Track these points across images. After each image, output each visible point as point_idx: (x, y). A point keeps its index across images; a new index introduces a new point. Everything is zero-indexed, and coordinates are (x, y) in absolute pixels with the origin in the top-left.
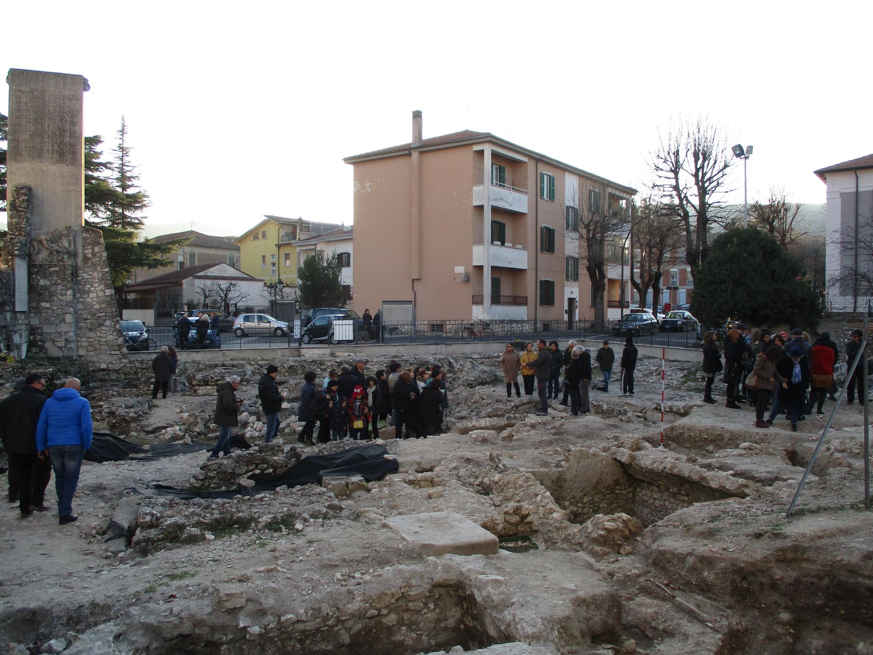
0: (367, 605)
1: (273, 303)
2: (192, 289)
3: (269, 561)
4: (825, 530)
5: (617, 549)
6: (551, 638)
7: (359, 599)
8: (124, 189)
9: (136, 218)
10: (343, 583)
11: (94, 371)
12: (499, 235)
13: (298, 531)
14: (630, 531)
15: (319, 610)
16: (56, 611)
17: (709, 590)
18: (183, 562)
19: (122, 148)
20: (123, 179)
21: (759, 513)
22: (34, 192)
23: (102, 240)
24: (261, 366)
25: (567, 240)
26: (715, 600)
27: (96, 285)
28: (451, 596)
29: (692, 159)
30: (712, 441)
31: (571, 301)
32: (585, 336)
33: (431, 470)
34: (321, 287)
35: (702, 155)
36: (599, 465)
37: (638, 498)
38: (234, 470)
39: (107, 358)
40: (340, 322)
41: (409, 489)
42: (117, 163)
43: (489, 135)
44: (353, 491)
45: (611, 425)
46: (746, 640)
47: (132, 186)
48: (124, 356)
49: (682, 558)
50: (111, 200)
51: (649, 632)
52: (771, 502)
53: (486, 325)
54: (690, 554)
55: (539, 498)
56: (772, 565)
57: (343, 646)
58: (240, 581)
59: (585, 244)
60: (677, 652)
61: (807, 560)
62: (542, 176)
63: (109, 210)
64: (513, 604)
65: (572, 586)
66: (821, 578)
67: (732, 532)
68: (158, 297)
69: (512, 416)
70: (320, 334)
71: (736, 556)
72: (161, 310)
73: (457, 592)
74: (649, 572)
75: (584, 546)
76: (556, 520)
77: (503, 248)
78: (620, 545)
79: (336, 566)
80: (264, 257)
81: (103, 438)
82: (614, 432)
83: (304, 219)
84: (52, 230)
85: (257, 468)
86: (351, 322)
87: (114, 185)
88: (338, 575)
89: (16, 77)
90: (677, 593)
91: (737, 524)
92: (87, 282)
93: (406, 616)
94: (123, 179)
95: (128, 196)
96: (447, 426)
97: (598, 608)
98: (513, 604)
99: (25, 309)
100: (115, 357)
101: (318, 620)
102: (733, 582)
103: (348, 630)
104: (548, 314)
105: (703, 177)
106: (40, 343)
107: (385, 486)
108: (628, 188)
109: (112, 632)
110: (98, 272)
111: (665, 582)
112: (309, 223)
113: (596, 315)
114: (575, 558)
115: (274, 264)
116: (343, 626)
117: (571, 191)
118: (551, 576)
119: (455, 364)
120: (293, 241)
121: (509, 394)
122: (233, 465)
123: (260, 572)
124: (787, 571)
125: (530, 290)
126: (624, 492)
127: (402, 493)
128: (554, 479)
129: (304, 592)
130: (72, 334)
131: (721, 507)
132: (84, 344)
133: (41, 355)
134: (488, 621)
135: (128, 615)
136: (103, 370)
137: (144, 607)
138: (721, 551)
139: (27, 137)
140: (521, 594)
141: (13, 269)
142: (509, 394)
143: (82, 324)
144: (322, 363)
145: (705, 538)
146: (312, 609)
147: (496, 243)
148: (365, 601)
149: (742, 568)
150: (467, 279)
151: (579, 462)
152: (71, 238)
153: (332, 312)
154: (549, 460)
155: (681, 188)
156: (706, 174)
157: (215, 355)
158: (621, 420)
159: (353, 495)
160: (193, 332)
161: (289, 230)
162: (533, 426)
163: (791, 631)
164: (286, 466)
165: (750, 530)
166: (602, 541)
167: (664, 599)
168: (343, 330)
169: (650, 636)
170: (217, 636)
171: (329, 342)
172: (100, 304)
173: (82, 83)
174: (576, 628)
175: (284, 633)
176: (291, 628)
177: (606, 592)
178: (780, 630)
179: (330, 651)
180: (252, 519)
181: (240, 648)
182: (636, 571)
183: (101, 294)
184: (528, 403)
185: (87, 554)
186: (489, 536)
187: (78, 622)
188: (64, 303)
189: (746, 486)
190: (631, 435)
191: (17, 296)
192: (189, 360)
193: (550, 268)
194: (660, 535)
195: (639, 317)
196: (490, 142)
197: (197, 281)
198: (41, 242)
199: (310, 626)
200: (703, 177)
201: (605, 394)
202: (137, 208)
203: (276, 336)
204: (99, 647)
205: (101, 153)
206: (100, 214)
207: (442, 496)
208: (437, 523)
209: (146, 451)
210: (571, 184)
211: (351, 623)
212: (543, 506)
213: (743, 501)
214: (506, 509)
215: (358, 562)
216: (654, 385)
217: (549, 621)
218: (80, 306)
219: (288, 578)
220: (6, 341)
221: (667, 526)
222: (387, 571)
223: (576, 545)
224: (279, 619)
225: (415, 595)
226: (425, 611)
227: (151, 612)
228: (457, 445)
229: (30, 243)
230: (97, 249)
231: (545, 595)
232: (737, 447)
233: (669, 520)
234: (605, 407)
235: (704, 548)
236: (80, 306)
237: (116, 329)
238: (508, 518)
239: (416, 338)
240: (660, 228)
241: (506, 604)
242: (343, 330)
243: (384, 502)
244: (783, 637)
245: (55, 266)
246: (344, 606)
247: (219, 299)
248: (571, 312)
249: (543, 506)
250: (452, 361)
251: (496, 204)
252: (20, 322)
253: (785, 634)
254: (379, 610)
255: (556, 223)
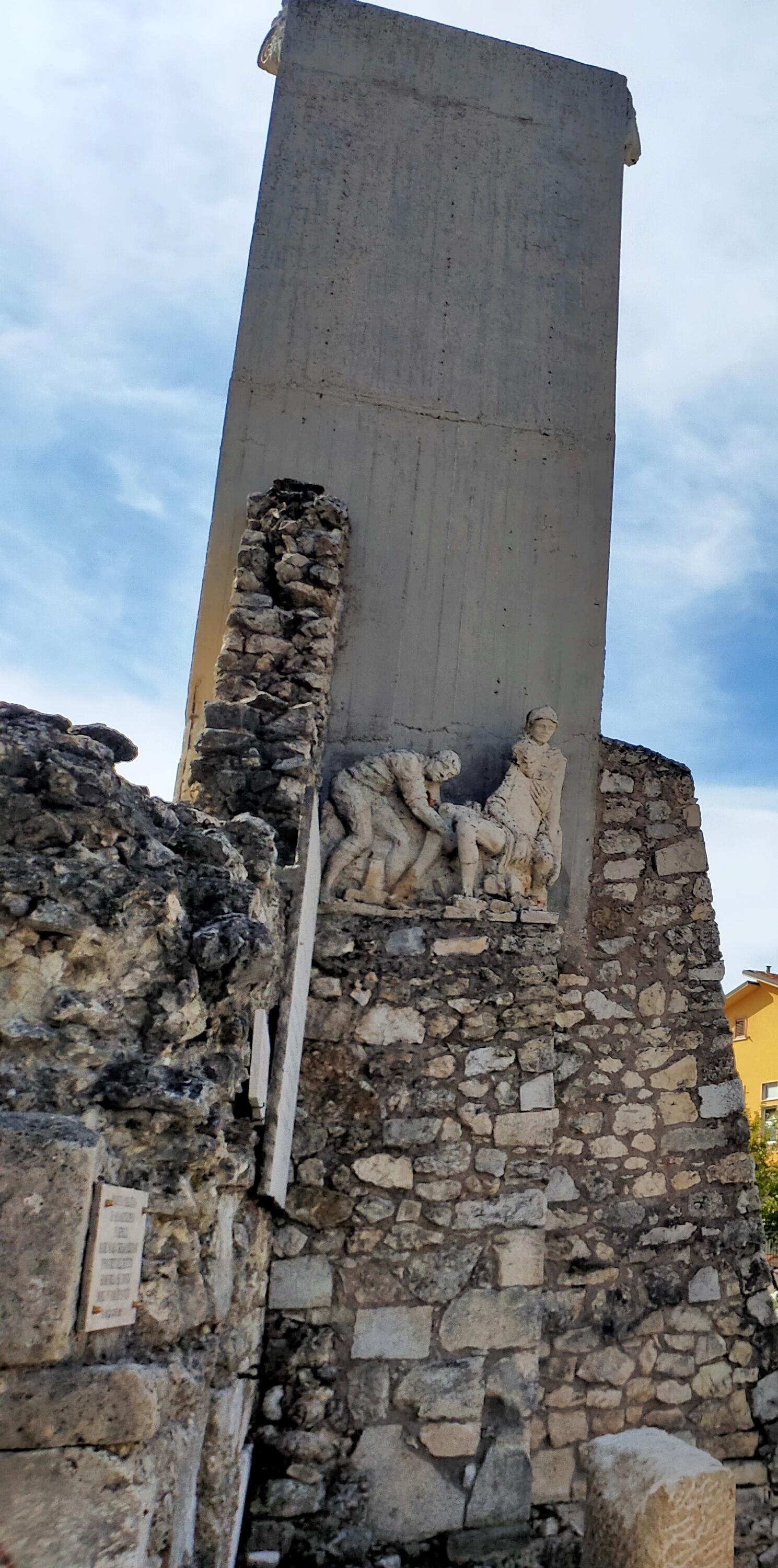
110: (669, 984)
172: (670, 1172)
183: (677, 1109)
188: (494, 1161)
237: (747, 1318)
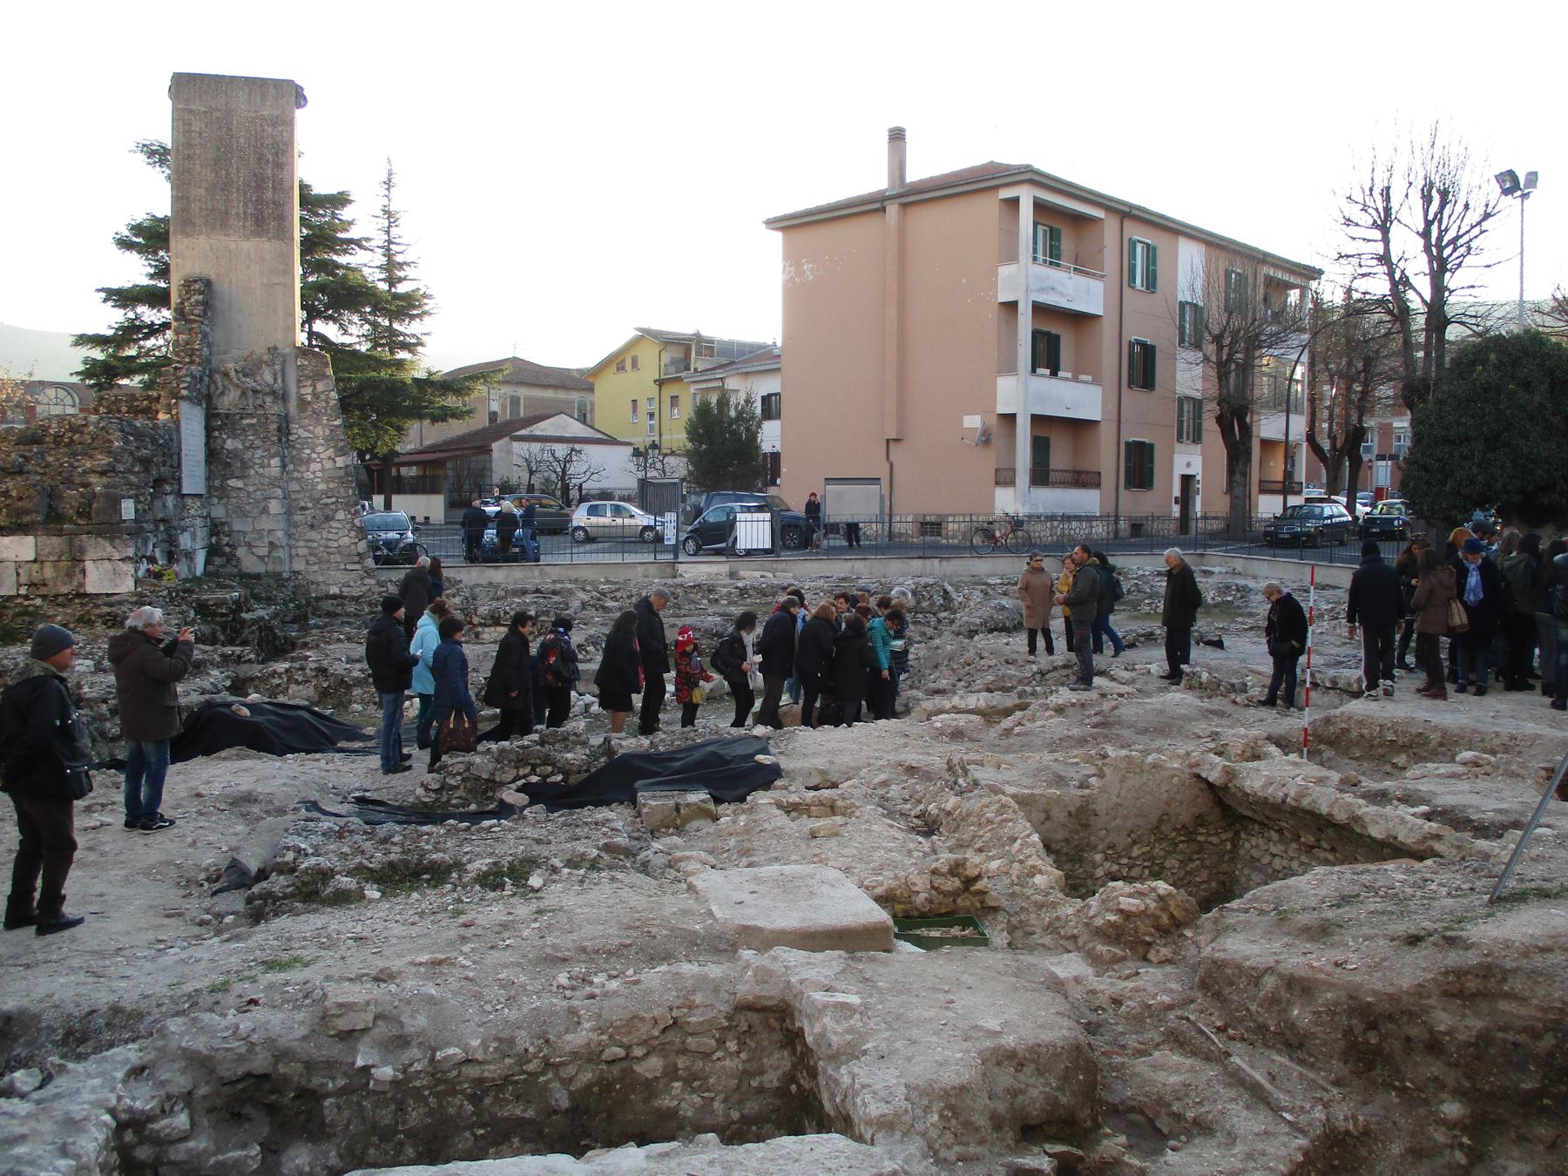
0: (604, 1037)
1: (643, 483)
2: (509, 459)
3: (451, 943)
4: (1559, 935)
5: (1142, 951)
6: (920, 1127)
7: (587, 1025)
8: (392, 285)
9: (414, 336)
10: (568, 993)
11: (318, 599)
12: (1047, 355)
13: (533, 890)
14: (1172, 917)
15: (511, 1042)
16: (48, 1018)
17: (1301, 1046)
18: (305, 939)
19: (388, 213)
20: (391, 268)
21: (1438, 891)
22: (216, 287)
23: (330, 371)
24: (603, 594)
25: (1180, 365)
26: (1312, 1066)
27: (320, 449)
28: (773, 1029)
29: (1417, 202)
30: (1404, 748)
31: (1187, 480)
32: (1206, 546)
33: (834, 786)
34: (727, 454)
35: (1438, 195)
36: (1164, 787)
37: (1242, 852)
38: (493, 774)
39: (341, 577)
40: (748, 516)
41: (781, 819)
42: (379, 239)
43: (1029, 169)
44: (687, 820)
45: (1213, 712)
46: (1364, 1152)
47: (405, 279)
48: (369, 573)
49: (1255, 977)
50: (369, 303)
51: (1164, 1125)
52: (1475, 871)
53: (1016, 523)
54: (1269, 970)
55: (1017, 845)
56: (1432, 1002)
57: (555, 1112)
58: (377, 979)
59: (1213, 373)
60: (1206, 1170)
61: (1510, 996)
62: (1132, 244)
63: (367, 321)
64: (865, 1053)
65: (994, 1024)
66: (1537, 1036)
67: (1366, 930)
68: (450, 473)
69: (1028, 689)
70: (714, 538)
71: (1358, 979)
72: (456, 497)
73: (775, 1020)
74: (1192, 1001)
75: (1081, 941)
76: (1037, 889)
77: (1054, 381)
78: (1149, 944)
79: (564, 960)
80: (634, 401)
81: (291, 713)
82: (1215, 725)
83: (704, 333)
84: (246, 353)
85: (533, 772)
86: (767, 516)
87: (375, 278)
88: (563, 979)
89: (183, 85)
90: (1237, 1046)
91: (1383, 913)
92: (305, 443)
93: (682, 1062)
94: (391, 268)
95: (396, 297)
96: (906, 705)
97: (1040, 1072)
98: (865, 1053)
99: (201, 489)
100: (353, 575)
101: (507, 1061)
102: (1348, 1032)
103: (566, 1082)
104: (1139, 504)
105: (1440, 238)
106: (227, 549)
107: (744, 812)
108: (1305, 267)
109: (127, 1061)
110: (324, 426)
111: (1219, 1024)
112: (712, 342)
113: (1233, 506)
114: (1030, 966)
115: (652, 415)
116: (556, 1074)
117: (1188, 272)
118: (963, 1000)
119: (954, 595)
120: (683, 375)
121: (1032, 649)
122: (491, 766)
123: (421, 964)
124: (1464, 1016)
125: (1107, 458)
126: (1215, 840)
127: (766, 825)
128: (1073, 809)
129: (488, 1008)
130: (280, 534)
131: (1365, 878)
132: (302, 551)
133: (230, 569)
134: (822, 1081)
135: (163, 1033)
136: (334, 597)
137: (194, 1019)
138: (1329, 968)
139: (203, 192)
140: (886, 1034)
141: (177, 422)
142: (1032, 649)
143: (298, 518)
144: (711, 590)
145: (1312, 939)
146: (497, 1039)
147: (1040, 371)
148: (601, 1030)
149: (1369, 1004)
150: (986, 439)
151: (1123, 780)
152: (277, 367)
153: (739, 499)
154: (1070, 773)
155: (1395, 260)
156: (1446, 230)
157: (529, 574)
158: (1234, 702)
159: (688, 827)
160: (490, 534)
161: (678, 354)
162: (1060, 710)
163: (1465, 1140)
164: (587, 771)
165: (1401, 928)
166: (1113, 934)
167: (1207, 1058)
168: (753, 530)
169: (1166, 1130)
170: (316, 1081)
171: (731, 552)
172: (327, 482)
173: (292, 94)
174: (979, 1110)
175: (439, 1081)
176: (455, 1073)
177: (1065, 1038)
178: (1440, 1136)
179: (531, 1121)
180: (458, 865)
181: (359, 1104)
182: (1166, 999)
183: (329, 465)
184: (1065, 667)
185: (168, 916)
186: (881, 915)
187: (82, 1040)
189: (1438, 837)
190: (1242, 731)
191: (184, 467)
192: (484, 582)
193: (1146, 418)
194: (1226, 929)
195: (1317, 511)
196: (1031, 182)
197: (515, 444)
198: (226, 374)
199: (492, 1071)
200: (1440, 238)
201: (1218, 654)
202: (413, 317)
203: (645, 542)
204: (93, 1090)
205: (351, 223)
206: (353, 329)
207: (837, 834)
208: (786, 886)
209: (370, 738)
210: (1189, 257)
211: (571, 1070)
212: (1021, 862)
213: (1417, 865)
214: (934, 865)
215: (610, 953)
216: (1324, 637)
217: (923, 1093)
218: (295, 486)
219: (467, 978)
220: (166, 545)
221: (1247, 911)
222: (654, 976)
223: (1068, 938)
224: (434, 1056)
225: (700, 1023)
226: (719, 1054)
227: (203, 1030)
228: (903, 740)
229: (210, 376)
230: (320, 387)
231: (934, 1039)
232: (1452, 760)
233: (1256, 899)
234: (1205, 676)
235: (1300, 959)
236: (295, 486)
238: (938, 881)
239: (893, 545)
240: (1368, 347)
241: (852, 1052)
242: (753, 530)
243: (732, 842)
244: (1447, 1152)
245: (251, 416)
246: (559, 1036)
247: (553, 477)
248: (1185, 500)
249: (1021, 862)
250: (949, 588)
251: (1041, 298)
252: (192, 512)
253: (1451, 1147)
254: (628, 1048)
255: (1159, 333)
